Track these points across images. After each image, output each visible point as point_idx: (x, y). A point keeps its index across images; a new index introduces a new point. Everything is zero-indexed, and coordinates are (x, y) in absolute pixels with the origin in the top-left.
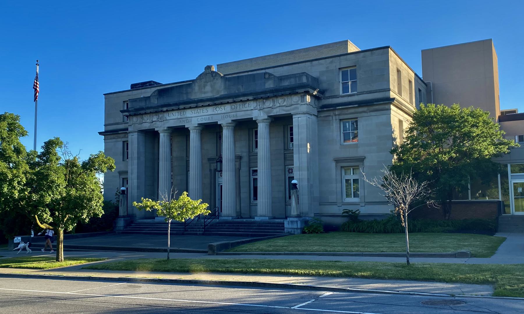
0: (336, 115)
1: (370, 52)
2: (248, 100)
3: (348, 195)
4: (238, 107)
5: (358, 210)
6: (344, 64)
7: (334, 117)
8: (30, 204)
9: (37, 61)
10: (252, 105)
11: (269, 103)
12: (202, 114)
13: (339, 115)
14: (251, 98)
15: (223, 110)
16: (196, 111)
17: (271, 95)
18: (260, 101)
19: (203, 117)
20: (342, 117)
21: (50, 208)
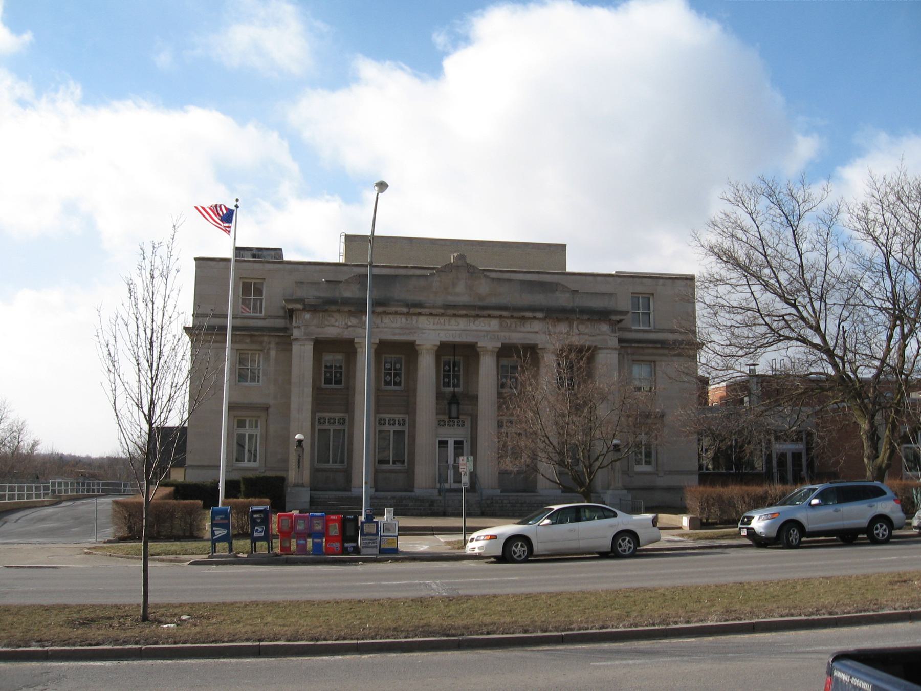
0: (628, 354)
1: (671, 281)
2: (535, 318)
3: (638, 462)
4: (514, 325)
5: (743, 498)
6: (640, 289)
7: (626, 356)
8: (847, 537)
9: (237, 200)
10: (537, 326)
11: (563, 328)
12: (447, 327)
13: (633, 354)
14: (540, 315)
15: (432, 324)
16: (436, 321)
17: (405, 310)
18: (321, 315)
19: (450, 332)
20: (636, 357)
21: (511, 502)
